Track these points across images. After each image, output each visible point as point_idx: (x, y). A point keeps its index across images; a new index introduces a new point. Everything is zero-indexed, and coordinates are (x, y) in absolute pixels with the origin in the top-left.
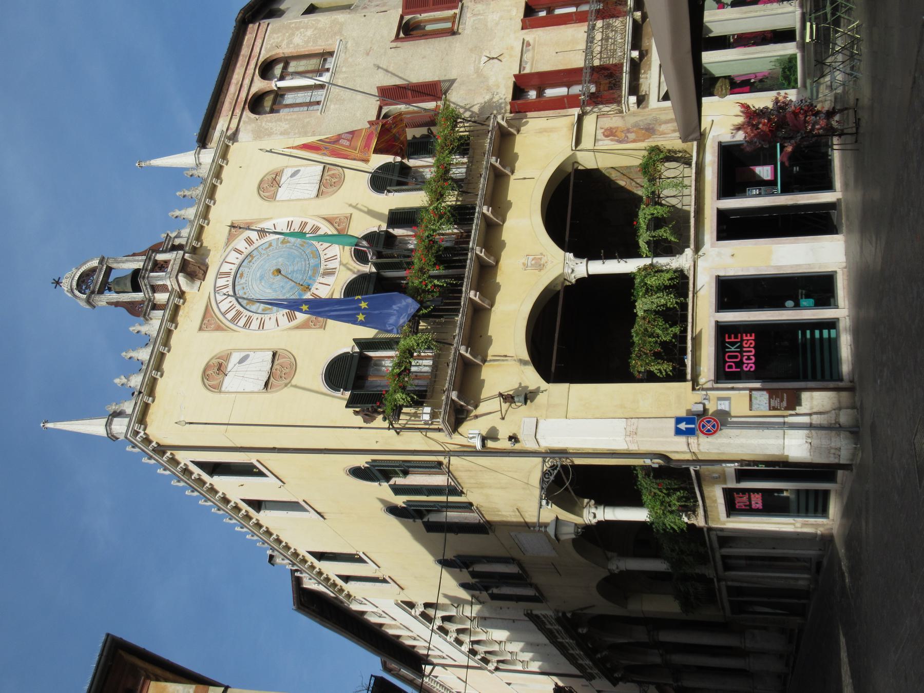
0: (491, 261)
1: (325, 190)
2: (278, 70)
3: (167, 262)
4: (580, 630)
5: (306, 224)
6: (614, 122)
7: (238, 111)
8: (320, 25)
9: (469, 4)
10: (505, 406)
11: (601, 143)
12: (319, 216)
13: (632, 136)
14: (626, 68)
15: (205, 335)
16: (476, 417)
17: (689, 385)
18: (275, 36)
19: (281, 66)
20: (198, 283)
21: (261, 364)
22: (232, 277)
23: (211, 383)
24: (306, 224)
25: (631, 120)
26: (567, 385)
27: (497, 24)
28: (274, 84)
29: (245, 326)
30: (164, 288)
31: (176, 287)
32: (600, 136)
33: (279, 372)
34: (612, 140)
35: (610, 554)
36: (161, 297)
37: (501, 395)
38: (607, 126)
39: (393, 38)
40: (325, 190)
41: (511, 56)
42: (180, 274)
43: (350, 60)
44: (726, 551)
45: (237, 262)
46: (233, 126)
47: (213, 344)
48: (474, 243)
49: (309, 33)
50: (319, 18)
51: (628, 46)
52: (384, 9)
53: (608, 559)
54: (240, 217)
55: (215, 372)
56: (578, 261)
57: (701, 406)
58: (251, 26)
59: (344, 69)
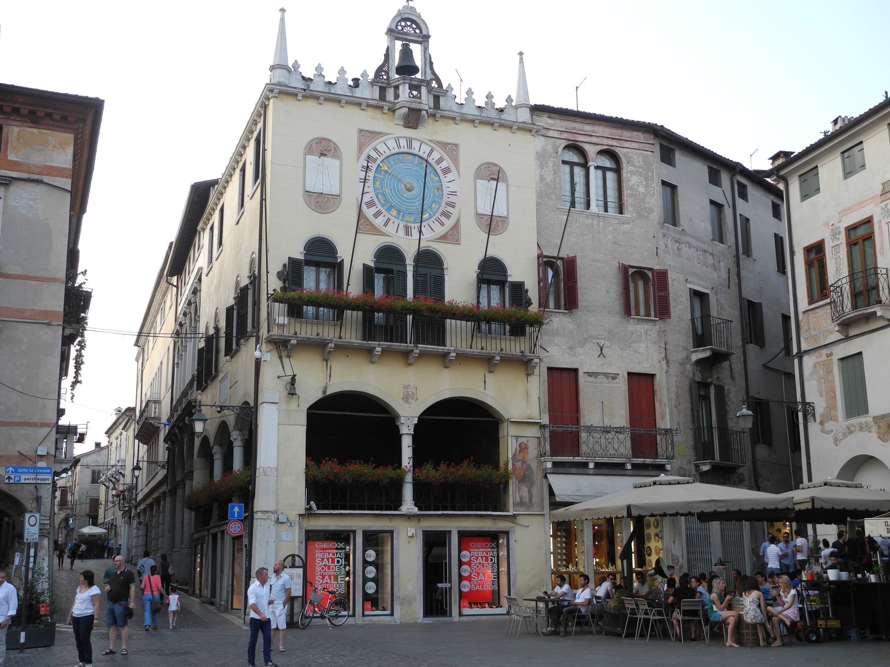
0: (411, 361)
2: (607, 163)
6: (533, 452)
7: (565, 136)
8: (648, 198)
11: (514, 441)
16: (280, 357)
18: (641, 159)
22: (408, 151)
24: (454, 207)
25: (534, 465)
27: (636, 352)
28: (592, 164)
30: (397, 96)
31: (397, 106)
32: (520, 440)
33: (322, 202)
37: (295, 376)
38: (529, 445)
39: (627, 263)
41: (603, 365)
42: (407, 110)
44: (219, 535)
45: (421, 153)
46: (551, 133)
47: (347, 142)
49: (641, 189)
51: (599, 460)
52: (660, 252)
57: (285, 520)
58: (652, 136)
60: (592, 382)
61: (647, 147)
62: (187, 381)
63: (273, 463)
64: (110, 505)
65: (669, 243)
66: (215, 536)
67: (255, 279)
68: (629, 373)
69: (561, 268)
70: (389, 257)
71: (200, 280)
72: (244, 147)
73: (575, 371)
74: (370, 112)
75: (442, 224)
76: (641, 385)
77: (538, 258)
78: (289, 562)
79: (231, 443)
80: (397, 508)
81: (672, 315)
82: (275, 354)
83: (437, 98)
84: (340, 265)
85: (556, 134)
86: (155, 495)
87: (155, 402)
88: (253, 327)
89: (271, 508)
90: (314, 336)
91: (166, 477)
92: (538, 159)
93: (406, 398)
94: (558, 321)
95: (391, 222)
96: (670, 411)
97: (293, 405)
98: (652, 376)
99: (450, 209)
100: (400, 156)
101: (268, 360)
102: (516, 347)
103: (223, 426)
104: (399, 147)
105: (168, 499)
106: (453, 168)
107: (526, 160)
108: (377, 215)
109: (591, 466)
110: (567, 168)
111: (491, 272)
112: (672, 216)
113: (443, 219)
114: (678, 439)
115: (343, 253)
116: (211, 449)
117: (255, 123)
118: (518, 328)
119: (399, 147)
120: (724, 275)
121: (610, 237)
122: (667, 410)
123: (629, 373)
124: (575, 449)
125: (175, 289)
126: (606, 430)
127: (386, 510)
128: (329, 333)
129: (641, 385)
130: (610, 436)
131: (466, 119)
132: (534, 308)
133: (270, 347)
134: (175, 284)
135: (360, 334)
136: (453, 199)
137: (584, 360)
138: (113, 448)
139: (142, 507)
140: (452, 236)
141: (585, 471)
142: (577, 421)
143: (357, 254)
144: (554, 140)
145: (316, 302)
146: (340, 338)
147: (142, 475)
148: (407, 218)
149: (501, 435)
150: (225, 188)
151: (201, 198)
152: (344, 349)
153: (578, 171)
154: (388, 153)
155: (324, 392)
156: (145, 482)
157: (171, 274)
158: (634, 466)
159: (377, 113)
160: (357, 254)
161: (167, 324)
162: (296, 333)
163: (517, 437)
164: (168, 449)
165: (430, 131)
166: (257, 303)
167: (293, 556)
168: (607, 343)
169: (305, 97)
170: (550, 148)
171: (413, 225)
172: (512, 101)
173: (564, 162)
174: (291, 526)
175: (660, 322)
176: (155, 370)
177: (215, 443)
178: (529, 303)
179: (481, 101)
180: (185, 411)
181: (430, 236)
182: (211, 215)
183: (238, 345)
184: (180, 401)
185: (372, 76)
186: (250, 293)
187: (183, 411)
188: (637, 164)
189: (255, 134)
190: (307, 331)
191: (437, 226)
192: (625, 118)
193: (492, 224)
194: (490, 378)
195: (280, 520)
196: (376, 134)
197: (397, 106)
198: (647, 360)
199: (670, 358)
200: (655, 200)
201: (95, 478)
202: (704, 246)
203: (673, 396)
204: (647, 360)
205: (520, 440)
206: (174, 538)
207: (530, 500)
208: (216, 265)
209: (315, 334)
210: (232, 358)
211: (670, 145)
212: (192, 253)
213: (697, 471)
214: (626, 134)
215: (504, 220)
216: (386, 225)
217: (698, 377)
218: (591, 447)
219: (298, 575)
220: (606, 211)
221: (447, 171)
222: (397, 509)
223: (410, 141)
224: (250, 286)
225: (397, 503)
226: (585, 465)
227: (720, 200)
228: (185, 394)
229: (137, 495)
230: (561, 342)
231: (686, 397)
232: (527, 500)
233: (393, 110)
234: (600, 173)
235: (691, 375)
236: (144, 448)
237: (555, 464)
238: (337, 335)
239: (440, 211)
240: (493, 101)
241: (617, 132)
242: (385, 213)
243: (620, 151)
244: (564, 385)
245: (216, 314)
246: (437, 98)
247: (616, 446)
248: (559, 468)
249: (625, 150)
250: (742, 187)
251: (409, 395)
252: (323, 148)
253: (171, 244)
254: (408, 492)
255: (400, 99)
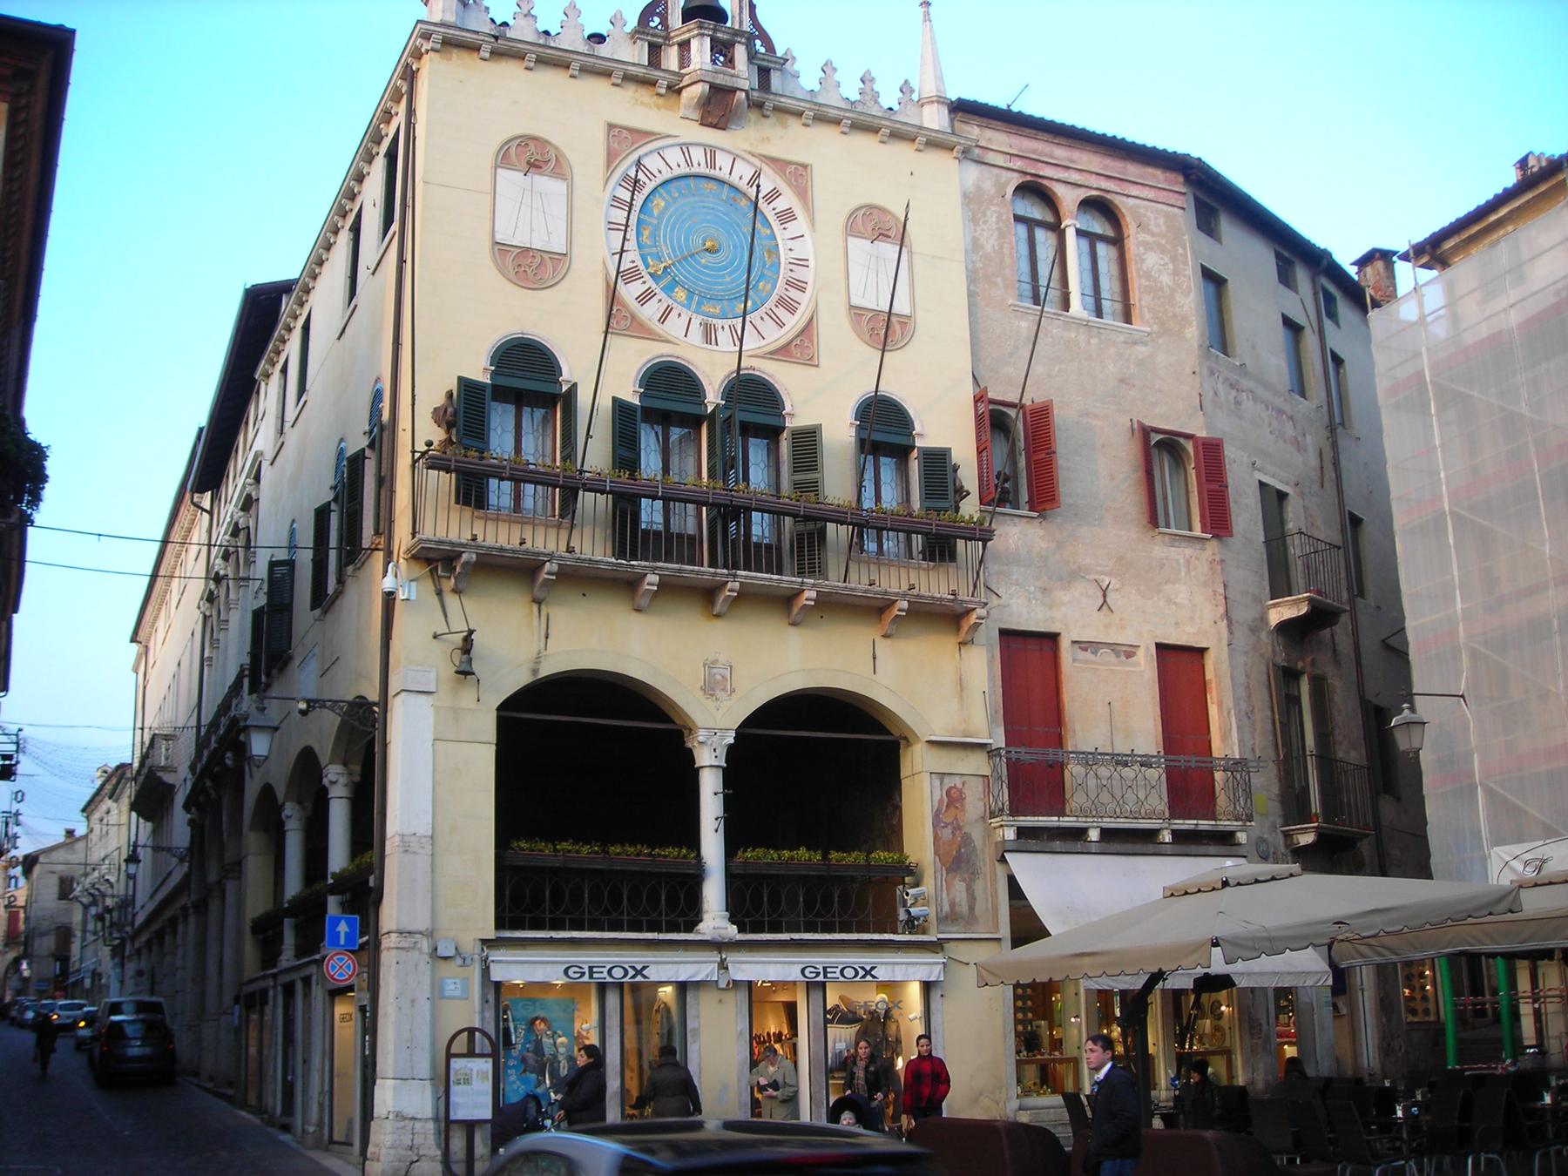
0: (718, 607)
1: (865, 319)
2: (1098, 226)
3: (730, 62)
4: (229, 755)
5: (803, 290)
6: (974, 804)
7: (1018, 164)
8: (1178, 297)
9: (1209, 552)
10: (458, 638)
11: (937, 783)
12: (815, 311)
13: (946, 834)
14: (1068, 822)
15: (600, 135)
16: (439, 593)
17: (491, 934)
18: (1161, 221)
19: (1110, 233)
20: (696, 115)
21: (546, 235)
22: (708, 172)
23: (513, 151)
24: (803, 290)
25: (977, 834)
26: (493, 739)
27: (1169, 601)
28: (1071, 224)
29: (615, 198)
30: (684, 60)
31: (686, 81)
32: (949, 782)
33: (529, 267)
34: (941, 801)
35: (309, 805)
36: (671, 59)
37: (471, 632)
38: (968, 793)
39: (1148, 422)
40: (865, 319)
41: (1108, 626)
42: (707, 87)
43: (1112, 351)
44: (299, 987)
45: (734, 179)
46: (991, 158)
47: (582, 144)
48: (746, 577)
49: (1166, 279)
50: (1192, 295)
51: (1109, 823)
52: (1207, 404)
53: (300, 802)
54: (820, 181)
55: (532, 156)
56: (722, 753)
57: (451, 952)
58: (1181, 179)
59: (1094, 341)
60: (1087, 662)
61: (1173, 198)
62: (230, 682)
63: (423, 826)
64: (90, 938)
65: (1221, 388)
66: (289, 989)
67: (382, 434)
68: (1160, 646)
69: (1020, 425)
70: (669, 384)
71: (257, 479)
72: (360, 178)
73: (1052, 638)
74: (631, 91)
75: (781, 325)
76: (1179, 665)
77: (976, 402)
78: (460, 1045)
79: (325, 791)
80: (691, 926)
81: (1235, 531)
82: (429, 586)
83: (764, 73)
84: (569, 398)
85: (1000, 160)
86: (168, 914)
87: (167, 738)
88: (377, 533)
89: (422, 923)
90: (515, 542)
91: (187, 877)
92: (968, 205)
93: (710, 688)
94: (1016, 534)
95: (674, 314)
96: (1230, 730)
97: (467, 697)
98: (1201, 652)
99: (794, 294)
100: (691, 182)
101: (413, 597)
102: (936, 584)
103: (308, 763)
104: (689, 163)
105: (192, 919)
106: (798, 211)
107: (943, 200)
108: (645, 298)
109: (1094, 835)
110: (1022, 230)
111: (883, 427)
112: (1220, 337)
113: (781, 312)
114: (1257, 780)
115: (575, 368)
116: (281, 808)
117: (387, 116)
118: (940, 549)
119: (689, 163)
120: (1314, 462)
121: (1111, 367)
122: (1233, 720)
123: (1160, 646)
124: (1056, 801)
125: (206, 516)
126: (1121, 761)
127: (668, 931)
128: (545, 541)
129: (1179, 665)
130: (1128, 772)
131: (823, 118)
132: (970, 508)
133: (420, 570)
134: (208, 507)
135: (609, 551)
136: (800, 273)
137: (1069, 615)
138: (94, 837)
139: (144, 938)
140: (800, 348)
141: (1079, 846)
142: (1059, 741)
143: (602, 375)
144: (996, 171)
145: (520, 476)
146: (570, 550)
147: (144, 870)
148: (708, 308)
149: (905, 771)
150: (315, 277)
151: (263, 315)
152: (579, 579)
153: (1044, 238)
154: (667, 175)
155: (535, 671)
156: (150, 890)
157: (200, 488)
158: (1179, 836)
159: (644, 94)
160: (602, 375)
161: (193, 566)
162: (474, 538)
163: (942, 775)
164: (191, 823)
165: (739, 151)
166: (385, 482)
167: (471, 1031)
168: (1115, 583)
169: (497, 54)
170: (988, 186)
171: (718, 323)
172: (912, 91)
173: (1018, 219)
174: (464, 965)
175: (1214, 543)
176: (168, 679)
177: (287, 798)
178: (961, 493)
179: (851, 90)
180: (221, 742)
181: (757, 346)
182: (284, 342)
183: (341, 581)
184: (214, 724)
185: (632, 23)
186: (370, 468)
187: (221, 741)
188: (1156, 230)
189: (386, 143)
190: (501, 536)
191: (768, 327)
192: (1129, 139)
193: (885, 330)
194: (884, 647)
195: (441, 952)
196: (642, 135)
197: (686, 81)
198: (1192, 618)
199: (1235, 616)
200: (1190, 301)
201: (66, 887)
202: (1279, 402)
203: (1242, 692)
204: (1192, 618)
205: (949, 782)
206: (203, 994)
207: (971, 908)
208: (292, 436)
209: (515, 542)
210: (325, 612)
211: (1213, 198)
212: (241, 438)
213: (1287, 846)
214: (1133, 170)
215: (906, 320)
216: (663, 319)
217: (1281, 660)
218: (1093, 796)
219: (483, 1075)
220: (1099, 313)
221: (787, 216)
222: (690, 929)
223: (711, 152)
224: (368, 453)
225: (690, 914)
226: (1079, 834)
227: (1300, 318)
228: (225, 707)
229: (134, 915)
230: (1029, 575)
231: (1261, 698)
232: (964, 909)
233: (675, 90)
234: (1085, 244)
235: (1269, 654)
236: (146, 827)
237: (1022, 832)
238: (563, 547)
239: (774, 298)
240: (876, 87)
241: (1114, 166)
242: (661, 295)
243: (1124, 205)
244: (1030, 660)
245: (292, 532)
246: (764, 73)
247: (1142, 795)
248: (1030, 838)
249: (1132, 201)
250: (1330, 299)
251: (716, 682)
252: (532, 156)
253: (201, 430)
254: (714, 893)
255: (692, 67)
